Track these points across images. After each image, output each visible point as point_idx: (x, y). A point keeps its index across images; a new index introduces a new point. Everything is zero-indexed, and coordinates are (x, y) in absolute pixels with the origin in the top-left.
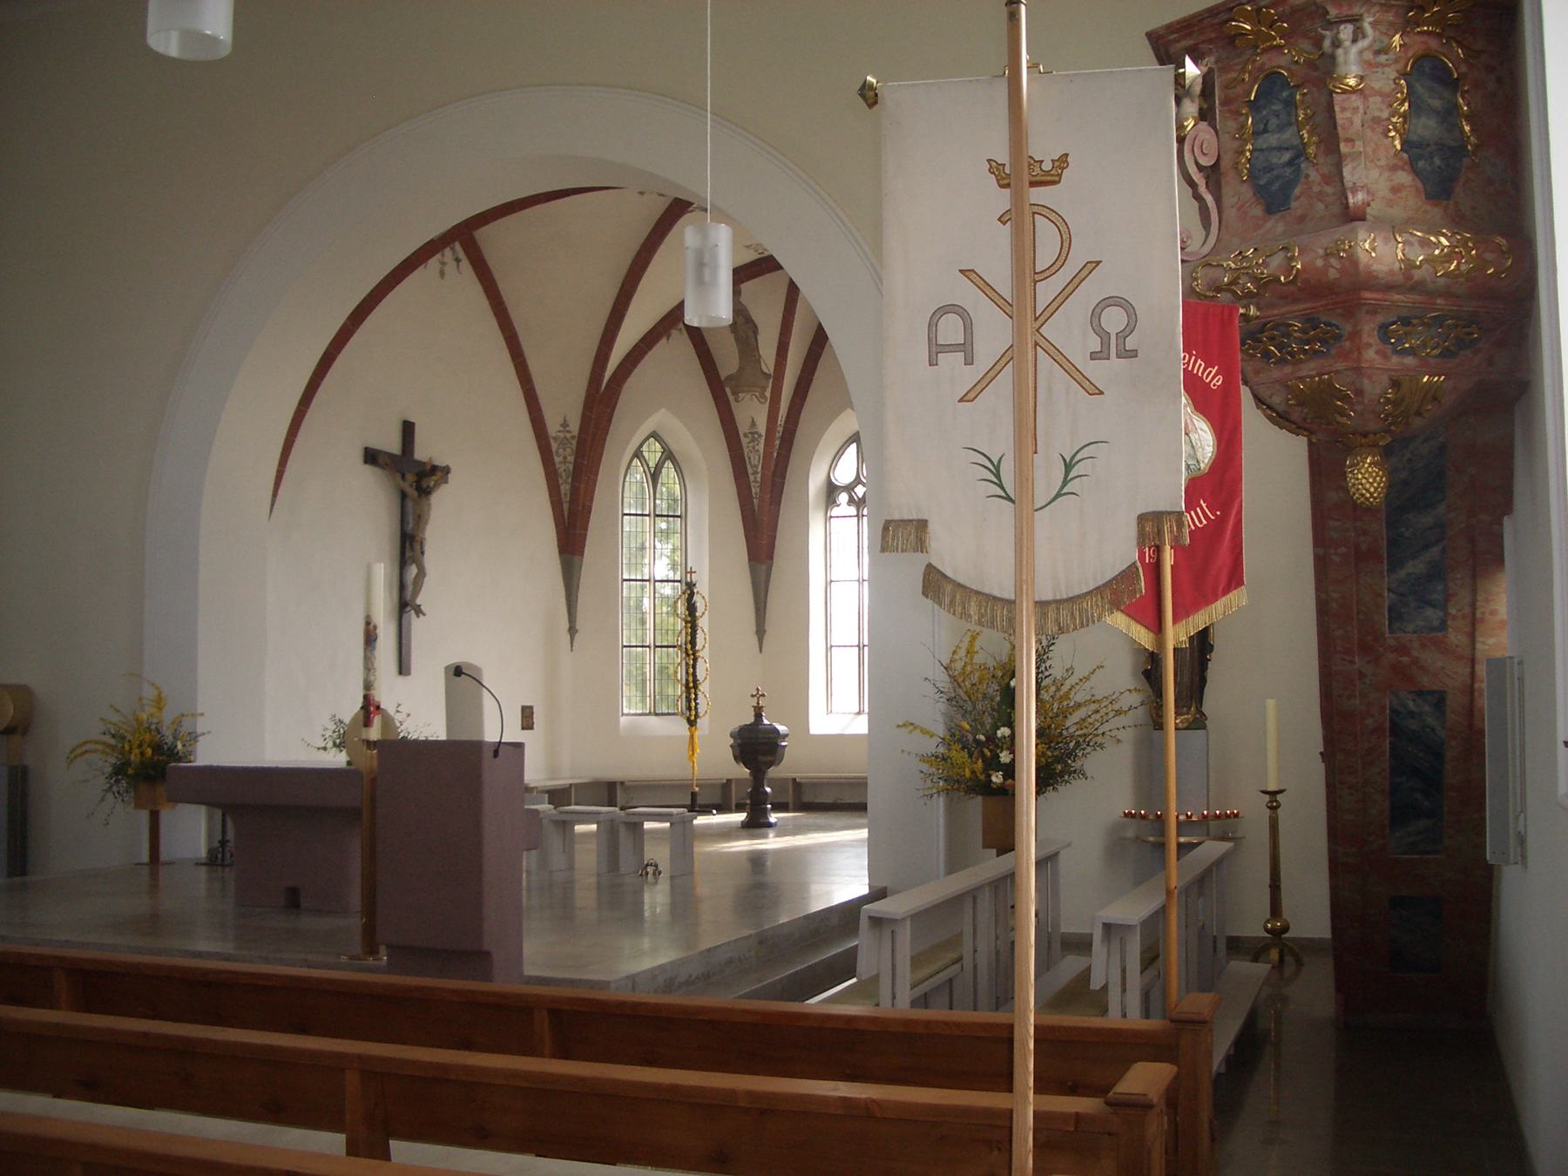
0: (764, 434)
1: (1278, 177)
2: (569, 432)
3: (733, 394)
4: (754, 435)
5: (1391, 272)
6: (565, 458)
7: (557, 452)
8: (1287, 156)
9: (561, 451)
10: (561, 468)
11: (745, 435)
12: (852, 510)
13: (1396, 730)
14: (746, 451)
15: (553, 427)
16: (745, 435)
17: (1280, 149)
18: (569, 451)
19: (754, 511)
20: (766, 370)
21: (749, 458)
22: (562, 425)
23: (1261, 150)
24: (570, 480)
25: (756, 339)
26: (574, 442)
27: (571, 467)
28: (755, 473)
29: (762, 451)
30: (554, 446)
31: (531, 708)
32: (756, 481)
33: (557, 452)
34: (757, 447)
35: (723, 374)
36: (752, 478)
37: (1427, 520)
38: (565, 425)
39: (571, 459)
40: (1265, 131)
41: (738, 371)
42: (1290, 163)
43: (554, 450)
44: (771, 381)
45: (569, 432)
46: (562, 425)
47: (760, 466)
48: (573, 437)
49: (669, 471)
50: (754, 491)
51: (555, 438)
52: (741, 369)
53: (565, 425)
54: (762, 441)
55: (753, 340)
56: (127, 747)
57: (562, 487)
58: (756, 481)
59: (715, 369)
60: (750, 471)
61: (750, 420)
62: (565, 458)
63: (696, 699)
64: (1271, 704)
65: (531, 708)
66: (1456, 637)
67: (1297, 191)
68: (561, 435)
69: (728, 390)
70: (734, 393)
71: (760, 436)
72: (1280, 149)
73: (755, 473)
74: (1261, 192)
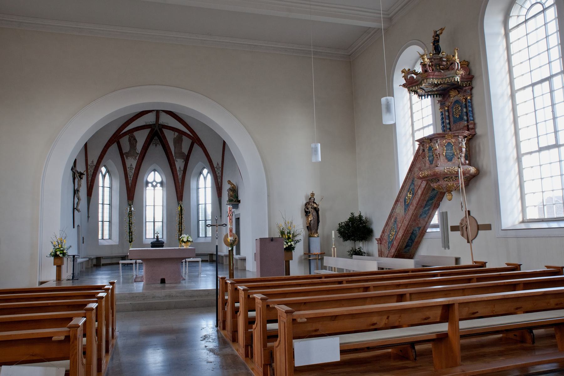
0: (135, 168)
1: (450, 157)
2: (93, 164)
3: (126, 157)
4: (131, 168)
5: (472, 173)
6: (91, 171)
7: (89, 169)
8: (452, 154)
9: (90, 169)
10: (89, 173)
11: (128, 168)
12: (153, 188)
13: (412, 233)
14: (128, 172)
15: (89, 163)
16: (128, 168)
17: (451, 153)
18: (92, 169)
19: (129, 188)
20: (137, 152)
21: (129, 174)
22: (92, 162)
23: (447, 153)
24: (91, 177)
25: (136, 145)
26: (94, 167)
27: (92, 173)
28: (130, 177)
29: (133, 172)
30: (89, 167)
31: (490, 229)
32: (130, 180)
33: (89, 169)
34: (132, 171)
35: (124, 152)
36: (129, 179)
37: (431, 202)
38: (93, 162)
39: (92, 171)
40: (448, 150)
41: (129, 152)
42: (452, 155)
43: (88, 168)
44: (139, 155)
45: (93, 164)
46: (92, 162)
47: (132, 176)
48: (94, 165)
49: (107, 176)
50: (129, 182)
51: (89, 165)
52: (130, 151)
53: (93, 162)
54: (134, 170)
55: (135, 145)
56: (382, 239)
57: (89, 178)
58: (130, 180)
59: (122, 150)
60: (129, 177)
61: (131, 164)
62: (91, 171)
63: (132, 236)
64: (333, 232)
65: (490, 229)
66: (426, 219)
67: (453, 159)
68: (91, 165)
69: (125, 156)
70: (127, 157)
71: (133, 168)
72: (451, 153)
73: (130, 177)
74: (447, 158)
